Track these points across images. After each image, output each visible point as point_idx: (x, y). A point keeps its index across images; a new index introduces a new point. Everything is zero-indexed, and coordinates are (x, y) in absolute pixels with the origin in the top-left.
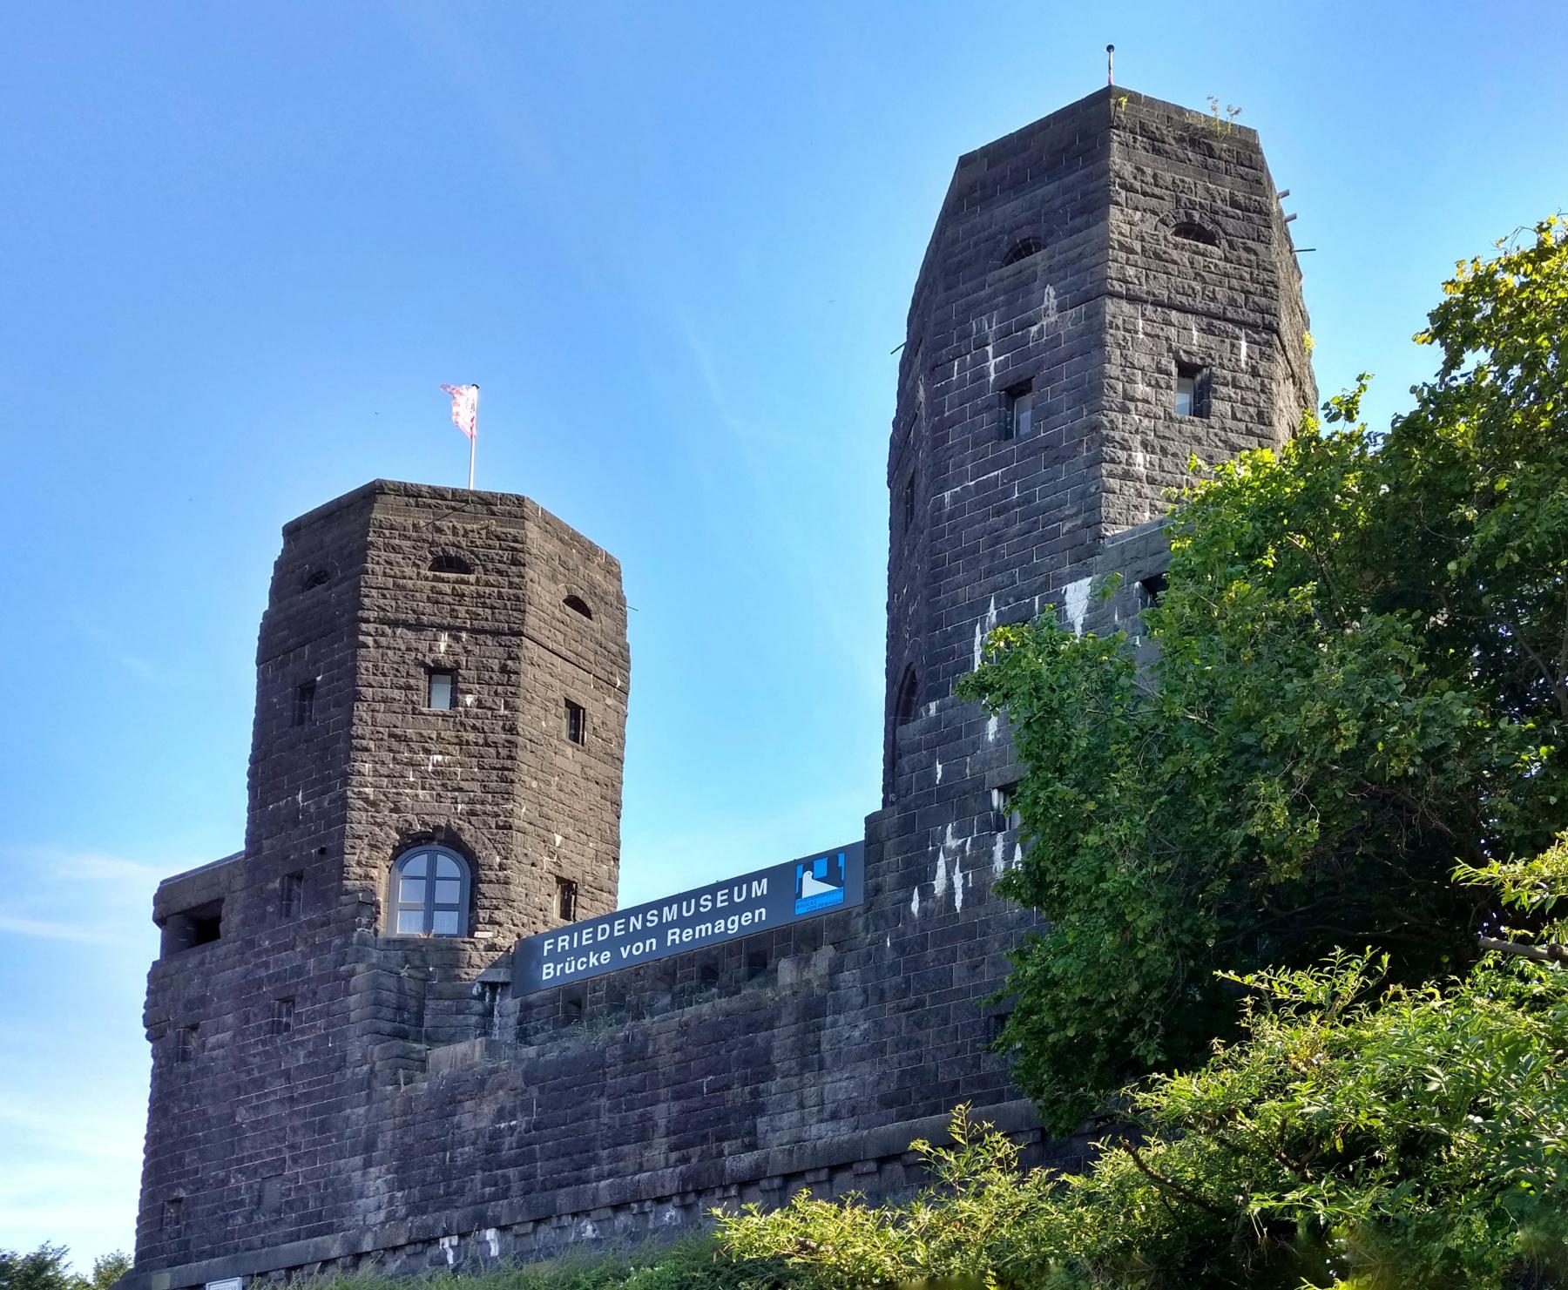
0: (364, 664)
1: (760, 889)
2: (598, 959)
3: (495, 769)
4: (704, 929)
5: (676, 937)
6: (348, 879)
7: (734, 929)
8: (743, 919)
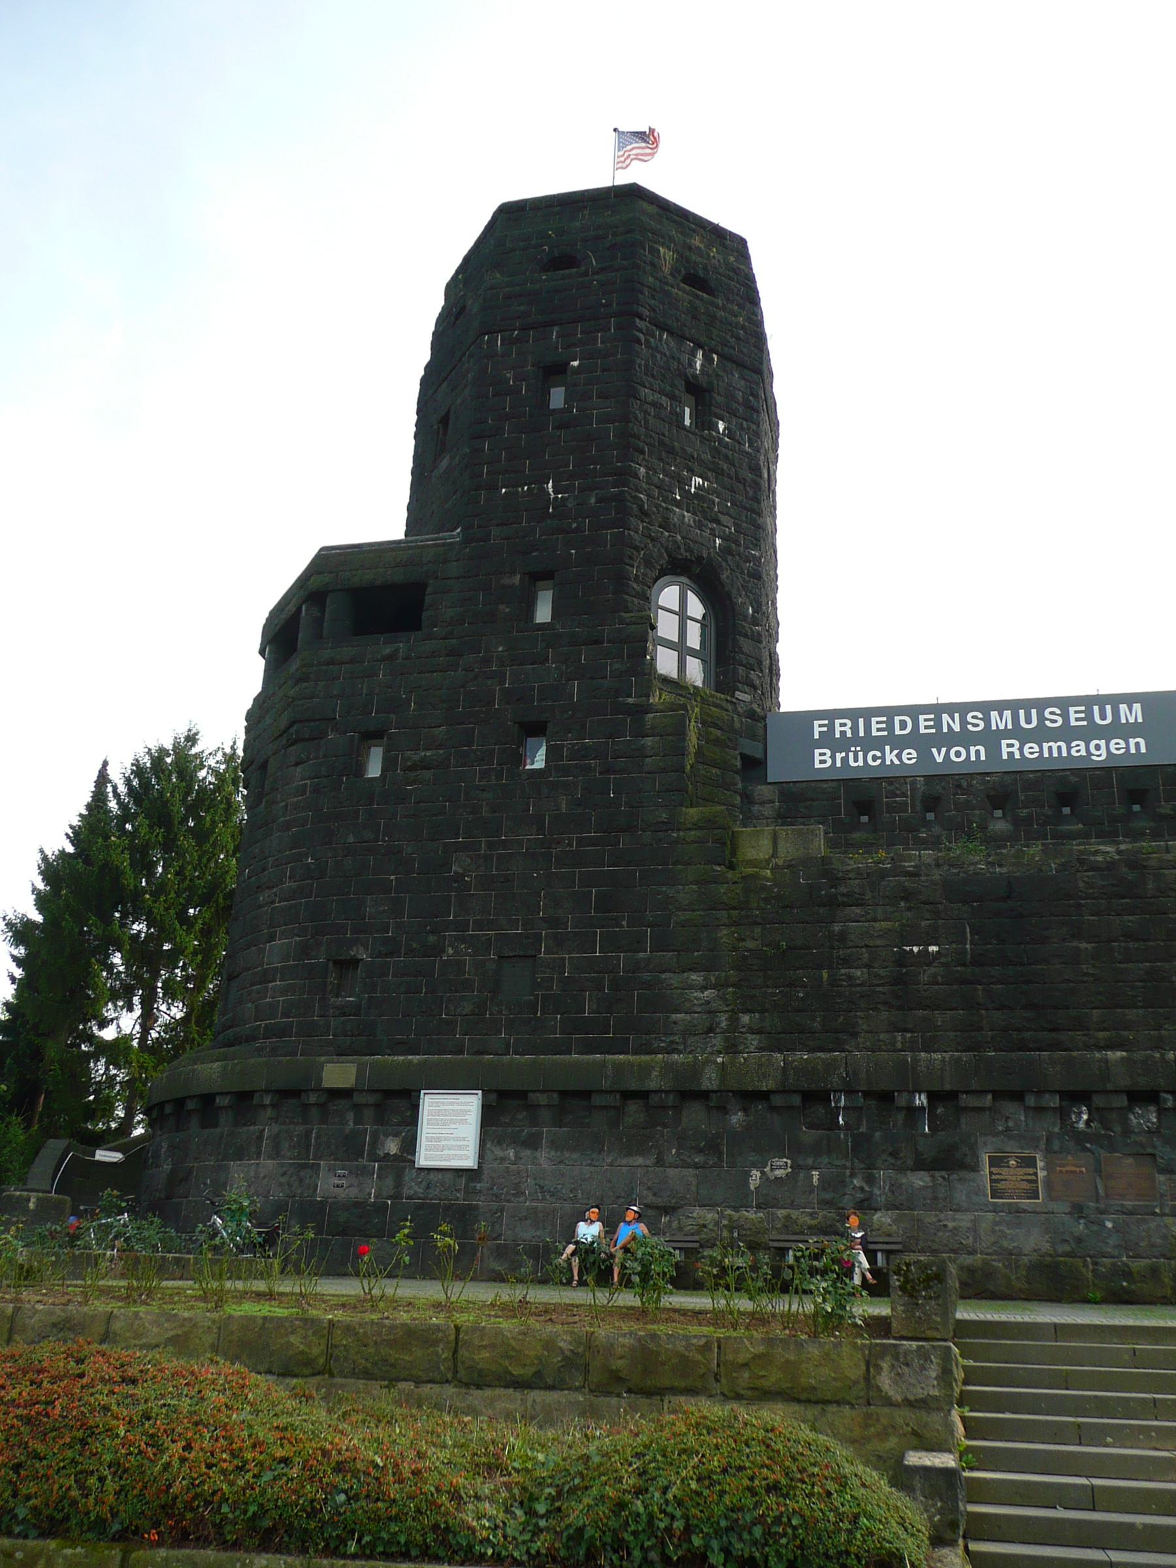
0: (639, 361)
1: (1133, 714)
2: (899, 756)
3: (745, 508)
4: (1054, 748)
5: (1015, 750)
6: (628, 594)
7: (1100, 756)
8: (953, 752)
